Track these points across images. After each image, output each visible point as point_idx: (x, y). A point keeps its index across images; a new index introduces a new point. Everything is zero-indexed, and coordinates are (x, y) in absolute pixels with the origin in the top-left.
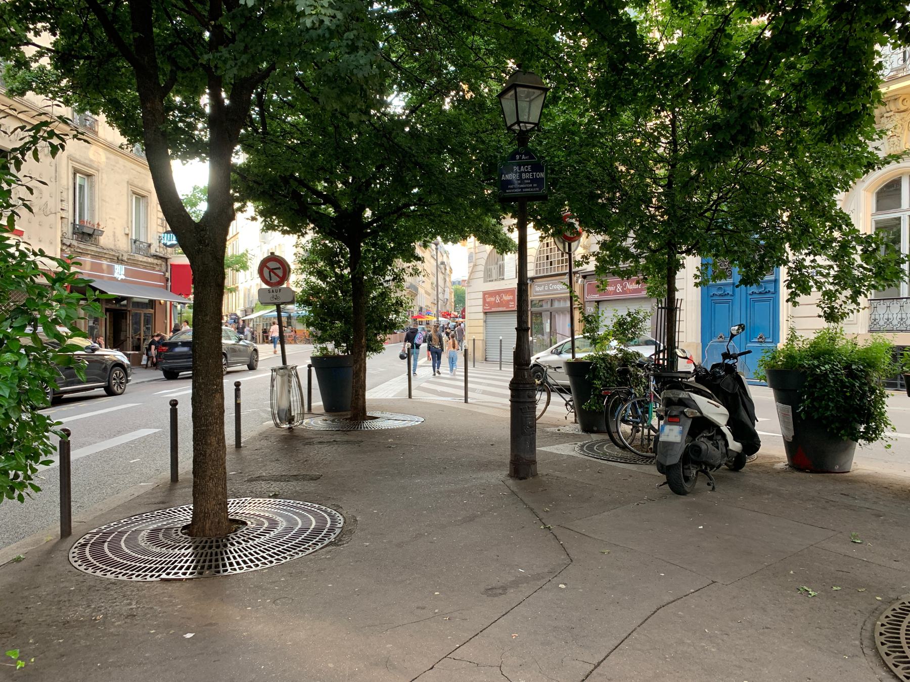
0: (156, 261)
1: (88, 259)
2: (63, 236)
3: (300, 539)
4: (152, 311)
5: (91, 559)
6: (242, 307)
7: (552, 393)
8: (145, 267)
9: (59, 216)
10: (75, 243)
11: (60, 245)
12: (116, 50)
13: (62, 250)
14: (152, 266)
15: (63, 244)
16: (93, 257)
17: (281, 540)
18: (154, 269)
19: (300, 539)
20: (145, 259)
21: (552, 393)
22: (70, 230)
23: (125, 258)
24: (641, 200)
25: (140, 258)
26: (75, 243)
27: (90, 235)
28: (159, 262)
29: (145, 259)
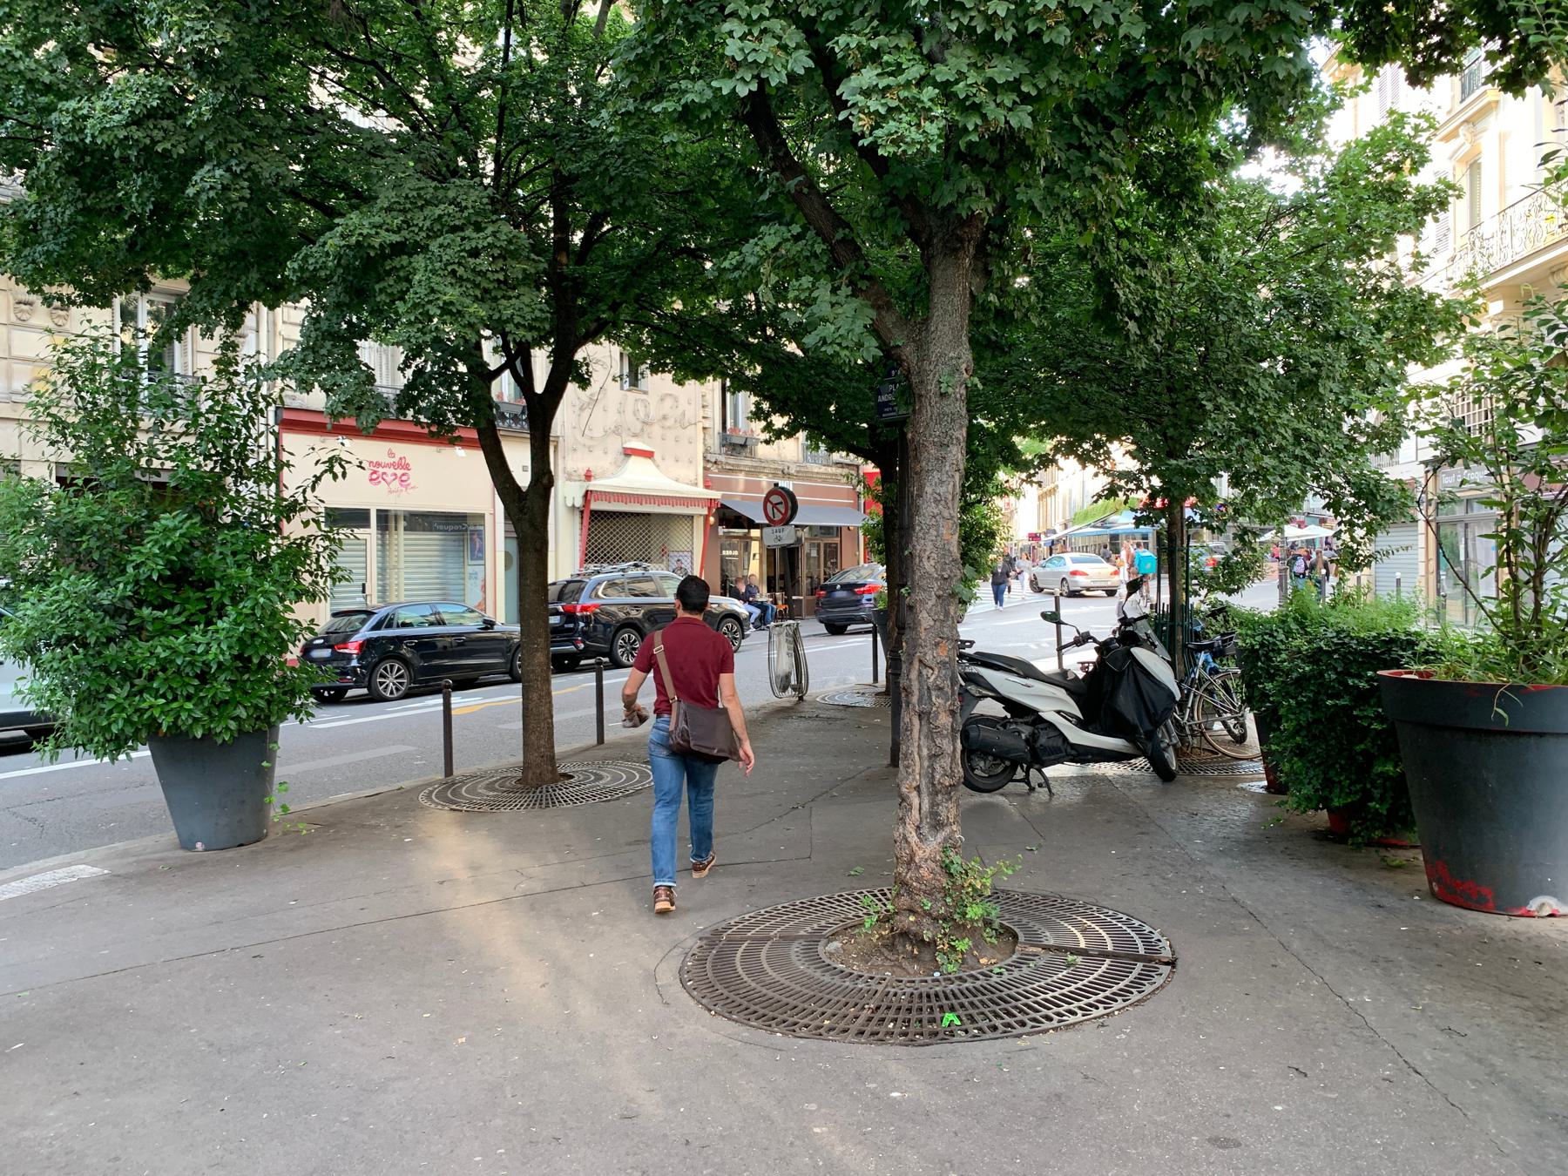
0: (839, 471)
1: (741, 477)
2: (706, 451)
3: (1091, 978)
4: (837, 540)
5: (1136, 937)
6: (1061, 520)
7: (605, 673)
8: (824, 481)
9: (700, 426)
10: (722, 458)
11: (701, 464)
12: (551, 215)
13: (705, 469)
14: (835, 478)
15: (706, 460)
16: (748, 473)
17: (1066, 990)
18: (838, 482)
19: (1091, 978)
20: (823, 470)
21: (605, 673)
22: (717, 441)
23: (792, 471)
24: (401, 151)
25: (816, 468)
26: (722, 458)
27: (744, 446)
28: (845, 471)
29: (823, 470)
